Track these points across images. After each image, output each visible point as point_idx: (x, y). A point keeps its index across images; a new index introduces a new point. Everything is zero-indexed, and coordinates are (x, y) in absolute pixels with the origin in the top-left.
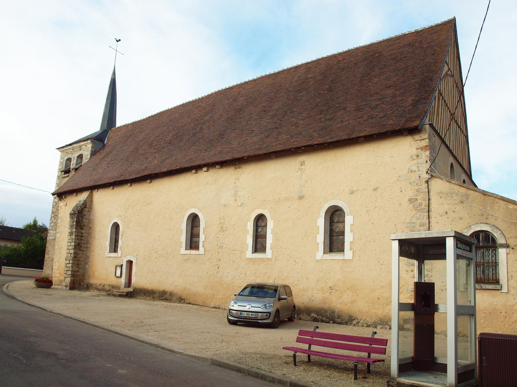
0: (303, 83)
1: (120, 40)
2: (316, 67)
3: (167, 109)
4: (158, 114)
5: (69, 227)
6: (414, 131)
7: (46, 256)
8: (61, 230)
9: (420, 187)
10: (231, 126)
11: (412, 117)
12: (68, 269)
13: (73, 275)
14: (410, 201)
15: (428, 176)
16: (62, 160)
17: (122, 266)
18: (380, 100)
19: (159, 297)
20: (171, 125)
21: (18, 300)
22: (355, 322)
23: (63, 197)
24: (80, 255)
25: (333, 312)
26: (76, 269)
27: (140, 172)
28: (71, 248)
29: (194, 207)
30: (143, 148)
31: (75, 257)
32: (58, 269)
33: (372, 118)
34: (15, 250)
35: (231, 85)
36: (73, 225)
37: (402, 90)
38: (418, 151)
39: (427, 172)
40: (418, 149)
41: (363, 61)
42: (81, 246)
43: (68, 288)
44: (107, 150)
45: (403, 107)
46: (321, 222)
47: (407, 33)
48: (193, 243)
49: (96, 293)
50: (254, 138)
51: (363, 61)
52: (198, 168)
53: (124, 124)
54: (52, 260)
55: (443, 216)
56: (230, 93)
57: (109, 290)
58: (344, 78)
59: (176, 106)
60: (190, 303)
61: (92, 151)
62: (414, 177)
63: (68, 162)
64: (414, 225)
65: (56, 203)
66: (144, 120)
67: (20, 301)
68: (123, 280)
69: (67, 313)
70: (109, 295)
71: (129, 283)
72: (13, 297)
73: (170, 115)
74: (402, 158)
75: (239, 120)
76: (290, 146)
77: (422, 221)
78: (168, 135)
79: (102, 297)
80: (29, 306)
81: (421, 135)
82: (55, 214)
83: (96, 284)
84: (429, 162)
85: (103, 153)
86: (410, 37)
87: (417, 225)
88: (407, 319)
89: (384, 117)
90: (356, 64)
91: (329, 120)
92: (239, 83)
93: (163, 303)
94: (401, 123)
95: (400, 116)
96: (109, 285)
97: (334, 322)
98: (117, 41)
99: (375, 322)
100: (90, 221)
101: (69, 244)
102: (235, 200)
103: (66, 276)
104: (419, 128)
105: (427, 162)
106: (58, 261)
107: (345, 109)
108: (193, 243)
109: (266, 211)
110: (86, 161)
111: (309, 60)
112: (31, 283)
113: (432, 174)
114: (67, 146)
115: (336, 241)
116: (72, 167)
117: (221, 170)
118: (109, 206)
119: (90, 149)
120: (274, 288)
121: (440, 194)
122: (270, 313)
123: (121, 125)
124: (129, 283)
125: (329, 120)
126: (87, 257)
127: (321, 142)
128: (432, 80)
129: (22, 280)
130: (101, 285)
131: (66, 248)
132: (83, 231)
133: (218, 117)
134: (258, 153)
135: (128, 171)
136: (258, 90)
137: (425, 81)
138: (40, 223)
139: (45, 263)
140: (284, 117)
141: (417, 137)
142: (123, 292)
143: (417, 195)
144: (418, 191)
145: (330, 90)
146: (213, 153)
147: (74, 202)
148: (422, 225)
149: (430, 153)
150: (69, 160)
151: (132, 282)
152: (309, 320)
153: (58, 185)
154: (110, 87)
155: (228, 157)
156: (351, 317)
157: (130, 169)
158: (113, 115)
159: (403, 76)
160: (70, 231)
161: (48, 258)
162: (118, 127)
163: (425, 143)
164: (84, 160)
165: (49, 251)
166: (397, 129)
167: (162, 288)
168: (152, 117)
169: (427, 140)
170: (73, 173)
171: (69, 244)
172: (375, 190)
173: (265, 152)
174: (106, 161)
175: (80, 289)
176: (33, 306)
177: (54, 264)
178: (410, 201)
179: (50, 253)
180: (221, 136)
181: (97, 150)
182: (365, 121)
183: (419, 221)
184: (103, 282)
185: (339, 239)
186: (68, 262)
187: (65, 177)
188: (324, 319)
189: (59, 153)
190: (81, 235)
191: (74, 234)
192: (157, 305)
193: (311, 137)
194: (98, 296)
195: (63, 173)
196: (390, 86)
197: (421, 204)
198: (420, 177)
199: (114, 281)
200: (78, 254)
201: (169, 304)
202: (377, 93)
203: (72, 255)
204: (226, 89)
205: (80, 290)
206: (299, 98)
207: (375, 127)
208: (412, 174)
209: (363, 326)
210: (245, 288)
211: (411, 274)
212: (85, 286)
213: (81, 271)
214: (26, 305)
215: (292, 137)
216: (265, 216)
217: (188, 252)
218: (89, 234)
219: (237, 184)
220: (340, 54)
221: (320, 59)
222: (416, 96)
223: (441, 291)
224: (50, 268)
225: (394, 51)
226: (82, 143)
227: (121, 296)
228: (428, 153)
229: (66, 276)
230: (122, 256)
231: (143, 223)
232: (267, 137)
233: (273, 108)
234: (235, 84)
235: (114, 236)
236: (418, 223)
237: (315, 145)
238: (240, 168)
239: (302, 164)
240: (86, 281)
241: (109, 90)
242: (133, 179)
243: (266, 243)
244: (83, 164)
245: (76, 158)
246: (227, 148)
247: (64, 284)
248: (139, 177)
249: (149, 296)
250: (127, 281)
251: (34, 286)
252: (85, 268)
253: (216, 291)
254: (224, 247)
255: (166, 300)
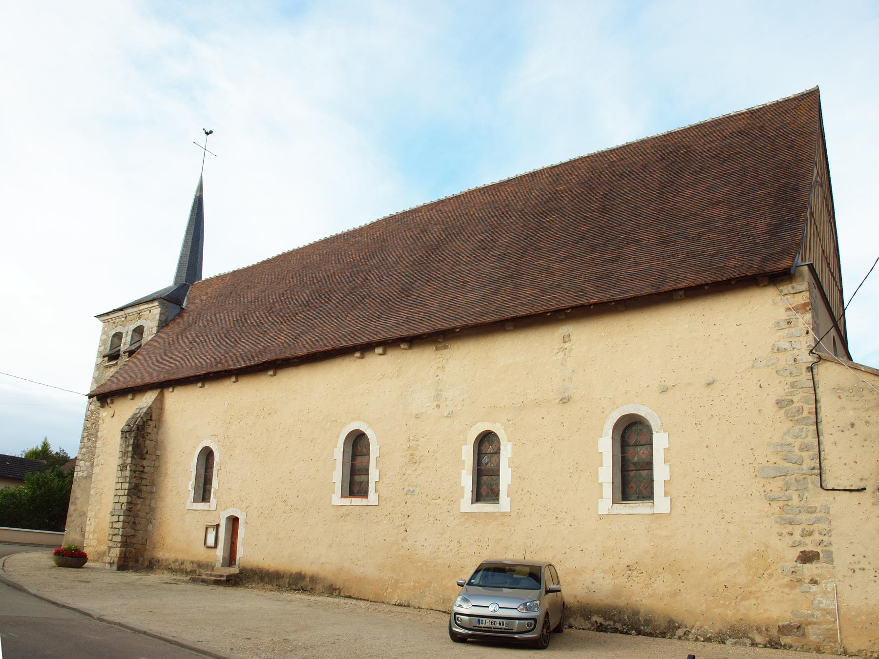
0: (550, 200)
1: (211, 132)
2: (571, 174)
3: (296, 248)
4: (279, 257)
5: (119, 455)
6: (778, 277)
7: (71, 508)
8: (102, 461)
9: (797, 379)
10: (422, 275)
11: (772, 254)
12: (116, 531)
13: (126, 543)
14: (780, 404)
15: (811, 359)
16: (105, 337)
17: (218, 526)
18: (704, 225)
19: (290, 585)
20: (306, 276)
21: (29, 593)
22: (680, 632)
23: (109, 401)
24: (138, 507)
25: (636, 613)
26: (130, 531)
27: (254, 357)
28: (121, 492)
29: (358, 419)
30: (257, 314)
31: (129, 510)
32: (94, 532)
33: (694, 256)
34: (13, 495)
35: (414, 206)
36: (128, 452)
37: (744, 209)
38: (789, 313)
39: (811, 351)
40: (789, 309)
41: (657, 161)
42: (140, 491)
43: (115, 567)
44: (187, 318)
45: (750, 236)
46: (606, 445)
47: (732, 114)
48: (356, 484)
49: (167, 576)
50: (471, 295)
51: (657, 161)
52: (366, 348)
53: (217, 274)
54: (84, 514)
55: (846, 431)
56: (413, 219)
57: (193, 572)
58: (626, 190)
59: (312, 242)
60: (350, 597)
61: (160, 320)
62: (784, 360)
63: (116, 340)
64: (789, 448)
65: (92, 412)
66: (254, 267)
67: (35, 595)
68: (220, 553)
69: (133, 621)
70: (194, 581)
71: (231, 558)
72: (18, 588)
73: (303, 259)
74: (757, 324)
75: (436, 264)
76: (543, 308)
77: (807, 440)
78: (302, 292)
79: (183, 586)
80: (54, 608)
81: (794, 284)
82: (91, 432)
83: (167, 560)
84: (811, 332)
85: (180, 324)
86: (739, 120)
87: (796, 449)
88: (784, 626)
89: (716, 254)
90: (645, 166)
91: (612, 261)
92: (428, 202)
93: (298, 596)
94: (755, 264)
95: (748, 251)
96: (192, 562)
97: (639, 633)
98: (207, 134)
99: (720, 632)
100: (158, 445)
101: (119, 486)
102: (438, 406)
103: (111, 544)
104: (792, 271)
105: (807, 333)
106: (95, 517)
107: (638, 242)
108: (356, 484)
109: (498, 425)
110: (150, 338)
111: (556, 162)
112: (45, 558)
113: (820, 354)
114: (115, 311)
115: (635, 480)
116: (123, 348)
117: (410, 351)
118: (193, 418)
119: (157, 317)
120: (528, 570)
121: (838, 391)
122: (534, 619)
123: (212, 276)
124: (231, 558)
125: (612, 261)
126: (152, 510)
127: (605, 299)
128: (797, 190)
129: (27, 551)
130: (176, 561)
131: (113, 493)
132: (145, 463)
133: (394, 259)
134: (482, 320)
135: (231, 354)
136: (466, 214)
137: (785, 192)
138: (54, 449)
139: (69, 519)
140: (522, 257)
141: (786, 288)
142: (221, 576)
143: (792, 394)
144: (793, 385)
145: (604, 210)
146: (392, 321)
147: (127, 410)
148: (805, 448)
149: (813, 317)
150: (118, 336)
151: (238, 557)
152: (589, 629)
153: (96, 380)
154: (192, 211)
155: (424, 328)
156: (671, 621)
157: (234, 351)
158: (197, 258)
159: (740, 184)
160: (120, 462)
161: (75, 510)
162: (207, 280)
163: (803, 298)
164: (145, 336)
165: (76, 498)
166: (750, 273)
167: (295, 568)
168: (269, 261)
169: (807, 294)
170: (124, 359)
171: (119, 486)
172: (709, 384)
173: (496, 318)
174: (187, 337)
175: (136, 570)
176: (63, 606)
177: (88, 522)
178: (780, 404)
179: (78, 502)
180: (405, 291)
181: (170, 319)
182: (682, 262)
183: (799, 440)
184: (181, 557)
185: (640, 476)
186: (116, 518)
187: (110, 367)
188: (619, 626)
189: (99, 325)
190: (141, 469)
191: (128, 468)
192: (291, 601)
193: (582, 291)
194: (176, 582)
195: (106, 359)
196: (719, 202)
197: (800, 410)
198: (795, 360)
199: (200, 554)
200: (136, 505)
201: (312, 598)
202: (695, 214)
203: (124, 507)
204: (405, 213)
205: (136, 571)
206: (546, 225)
207: (704, 271)
208: (779, 355)
209: (697, 639)
210: (477, 572)
211: (789, 540)
212: (147, 563)
213: (140, 535)
214: (48, 605)
215: (544, 291)
216: (495, 435)
217: (347, 501)
218: (156, 468)
219: (440, 377)
220: (612, 151)
221: (575, 160)
222: (773, 217)
223: (851, 572)
224: (78, 529)
225: (714, 145)
226: (142, 307)
227: (217, 582)
228: (808, 316)
229: (111, 544)
230: (219, 509)
231: (261, 449)
232: (495, 293)
233: (500, 243)
234: (420, 204)
235: (203, 471)
236: (797, 444)
237: (591, 305)
238: (445, 347)
239: (566, 339)
240: (148, 555)
241: (191, 216)
242: (241, 369)
243: (498, 484)
244: (143, 342)
245: (130, 333)
246: (419, 312)
247: (108, 559)
248: (254, 365)
249: (270, 582)
250: (227, 555)
251: (53, 563)
252: (146, 530)
253: (402, 574)
254: (416, 493)
255: (304, 590)
